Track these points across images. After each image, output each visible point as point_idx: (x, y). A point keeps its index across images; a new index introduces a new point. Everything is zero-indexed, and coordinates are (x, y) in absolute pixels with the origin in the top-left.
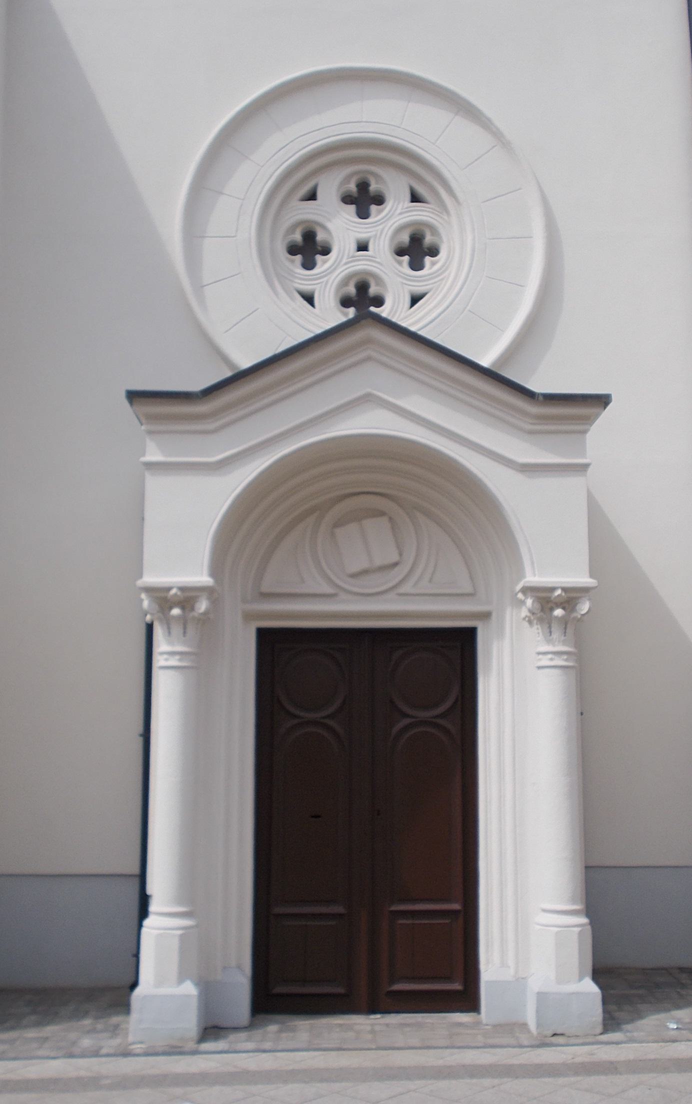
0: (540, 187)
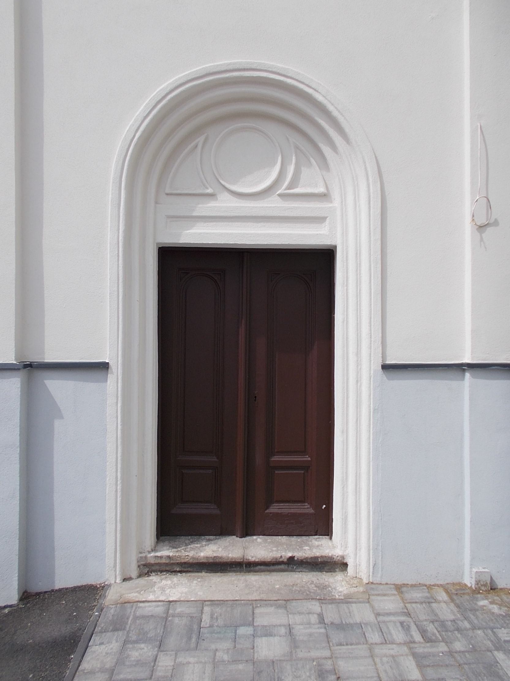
0: (376, 157)
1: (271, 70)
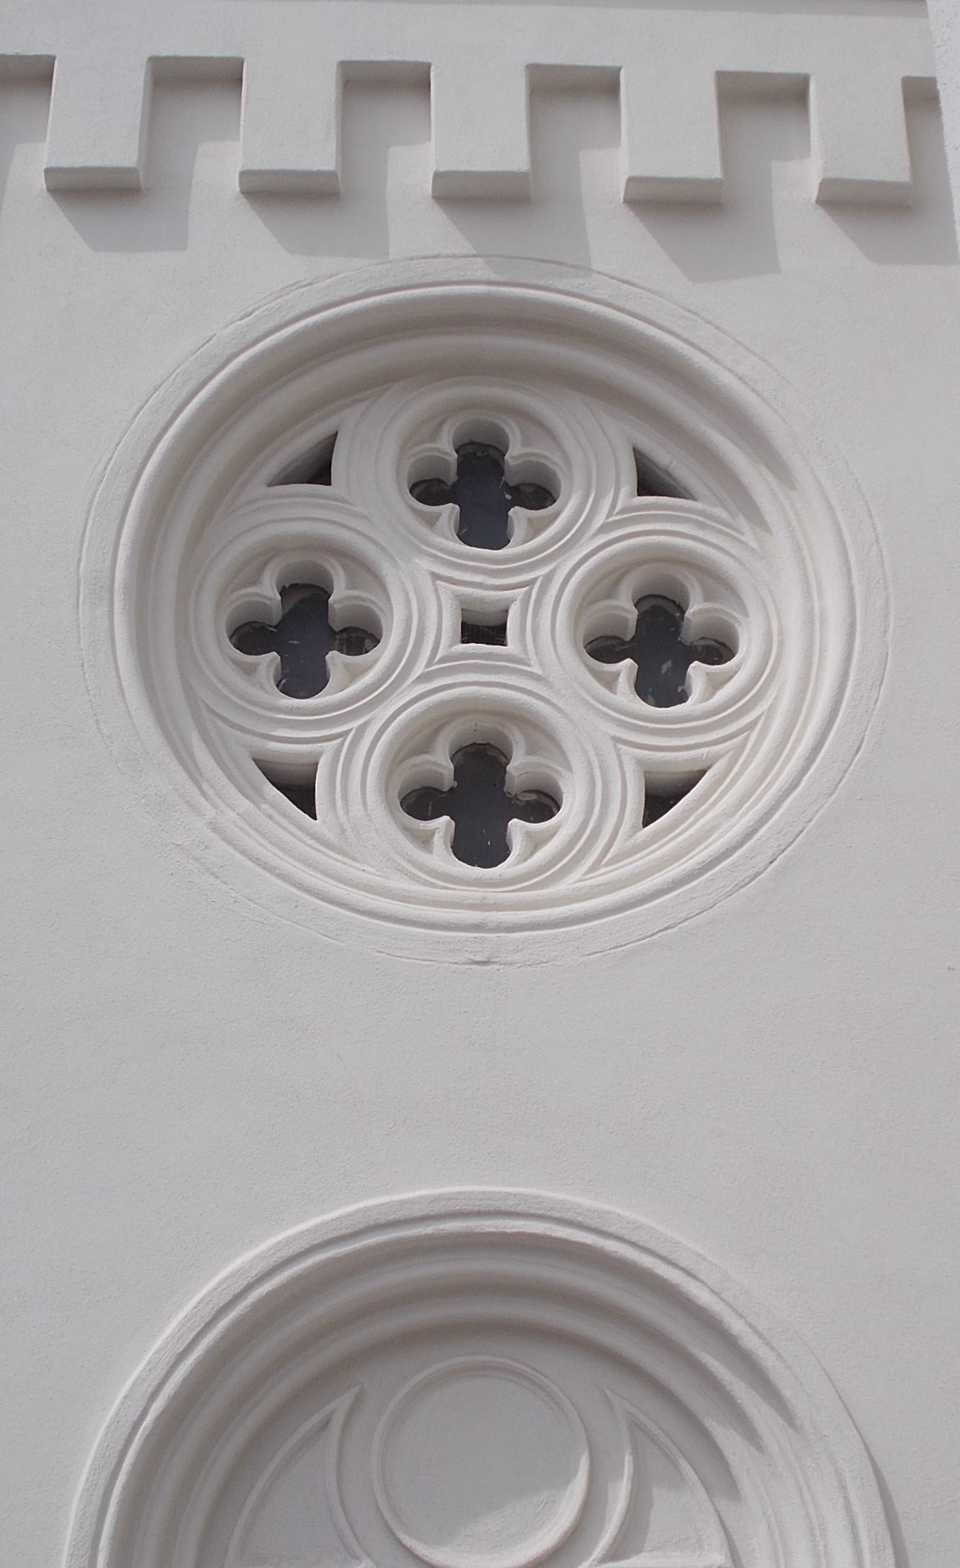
0: (876, 1471)
1: (556, 1214)
